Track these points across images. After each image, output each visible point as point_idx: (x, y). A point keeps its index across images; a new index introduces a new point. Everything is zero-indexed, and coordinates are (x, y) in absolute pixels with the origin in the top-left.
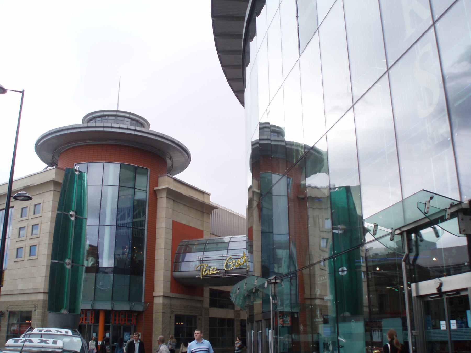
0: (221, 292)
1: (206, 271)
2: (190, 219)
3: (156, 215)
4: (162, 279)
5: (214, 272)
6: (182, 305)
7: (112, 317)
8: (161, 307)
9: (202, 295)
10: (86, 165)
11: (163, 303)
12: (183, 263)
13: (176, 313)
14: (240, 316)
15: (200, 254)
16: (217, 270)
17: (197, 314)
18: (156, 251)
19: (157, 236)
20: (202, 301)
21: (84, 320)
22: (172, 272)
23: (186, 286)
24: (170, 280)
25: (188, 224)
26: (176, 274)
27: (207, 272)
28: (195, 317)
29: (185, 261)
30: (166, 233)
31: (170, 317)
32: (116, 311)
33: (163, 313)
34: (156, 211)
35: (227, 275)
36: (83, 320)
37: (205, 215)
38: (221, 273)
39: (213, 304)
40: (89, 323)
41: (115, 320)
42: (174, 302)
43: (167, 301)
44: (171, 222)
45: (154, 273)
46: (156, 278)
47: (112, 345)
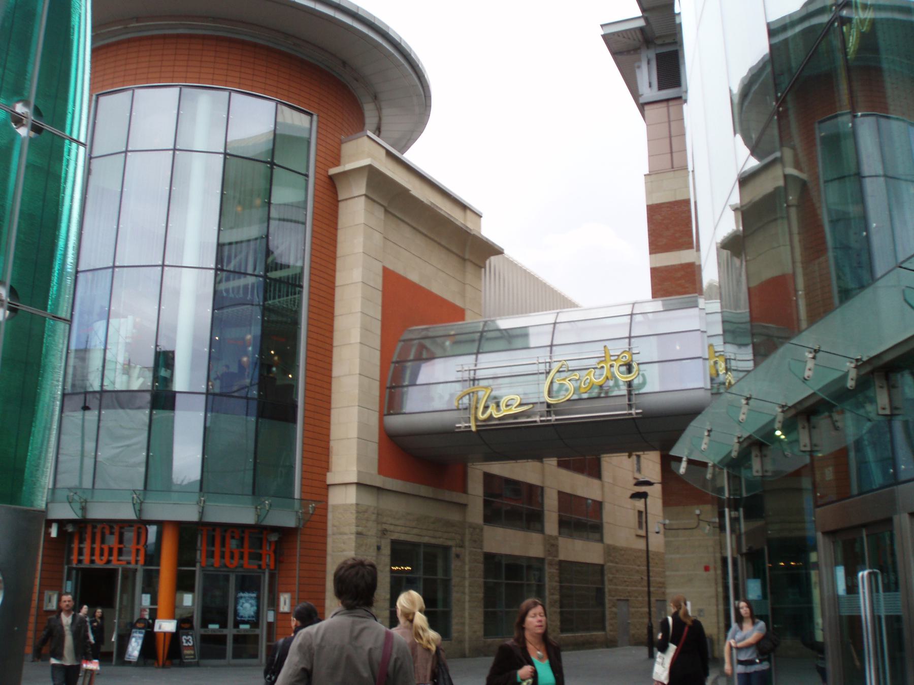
0: (514, 486)
1: (486, 407)
2: (428, 271)
3: (335, 247)
4: (353, 432)
5: (514, 410)
6: (411, 514)
7: (201, 543)
8: (351, 517)
9: (464, 490)
10: (125, 97)
11: (357, 504)
12: (410, 389)
13: (395, 536)
14: (557, 551)
15: (467, 361)
16: (521, 405)
17: (450, 543)
18: (336, 351)
19: (339, 309)
20: (463, 506)
21: (115, 552)
22: (382, 415)
23: (422, 458)
24: (376, 439)
25: (423, 285)
26: (395, 422)
27: (492, 410)
28: (446, 549)
29: (418, 382)
30: (366, 299)
31: (379, 548)
32: (215, 526)
33: (359, 534)
34: (336, 235)
35: (553, 418)
36: (110, 554)
37: (470, 268)
38: (534, 414)
39: (493, 515)
40: (129, 563)
41: (211, 555)
42: (390, 504)
43: (369, 500)
44: (380, 272)
45: (329, 416)
46: (336, 432)
47: (202, 631)
